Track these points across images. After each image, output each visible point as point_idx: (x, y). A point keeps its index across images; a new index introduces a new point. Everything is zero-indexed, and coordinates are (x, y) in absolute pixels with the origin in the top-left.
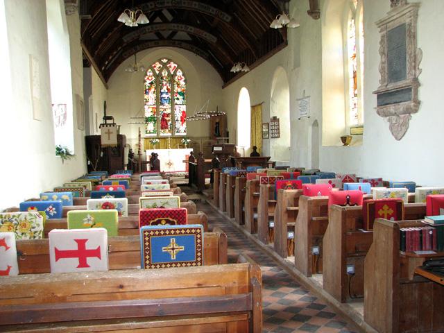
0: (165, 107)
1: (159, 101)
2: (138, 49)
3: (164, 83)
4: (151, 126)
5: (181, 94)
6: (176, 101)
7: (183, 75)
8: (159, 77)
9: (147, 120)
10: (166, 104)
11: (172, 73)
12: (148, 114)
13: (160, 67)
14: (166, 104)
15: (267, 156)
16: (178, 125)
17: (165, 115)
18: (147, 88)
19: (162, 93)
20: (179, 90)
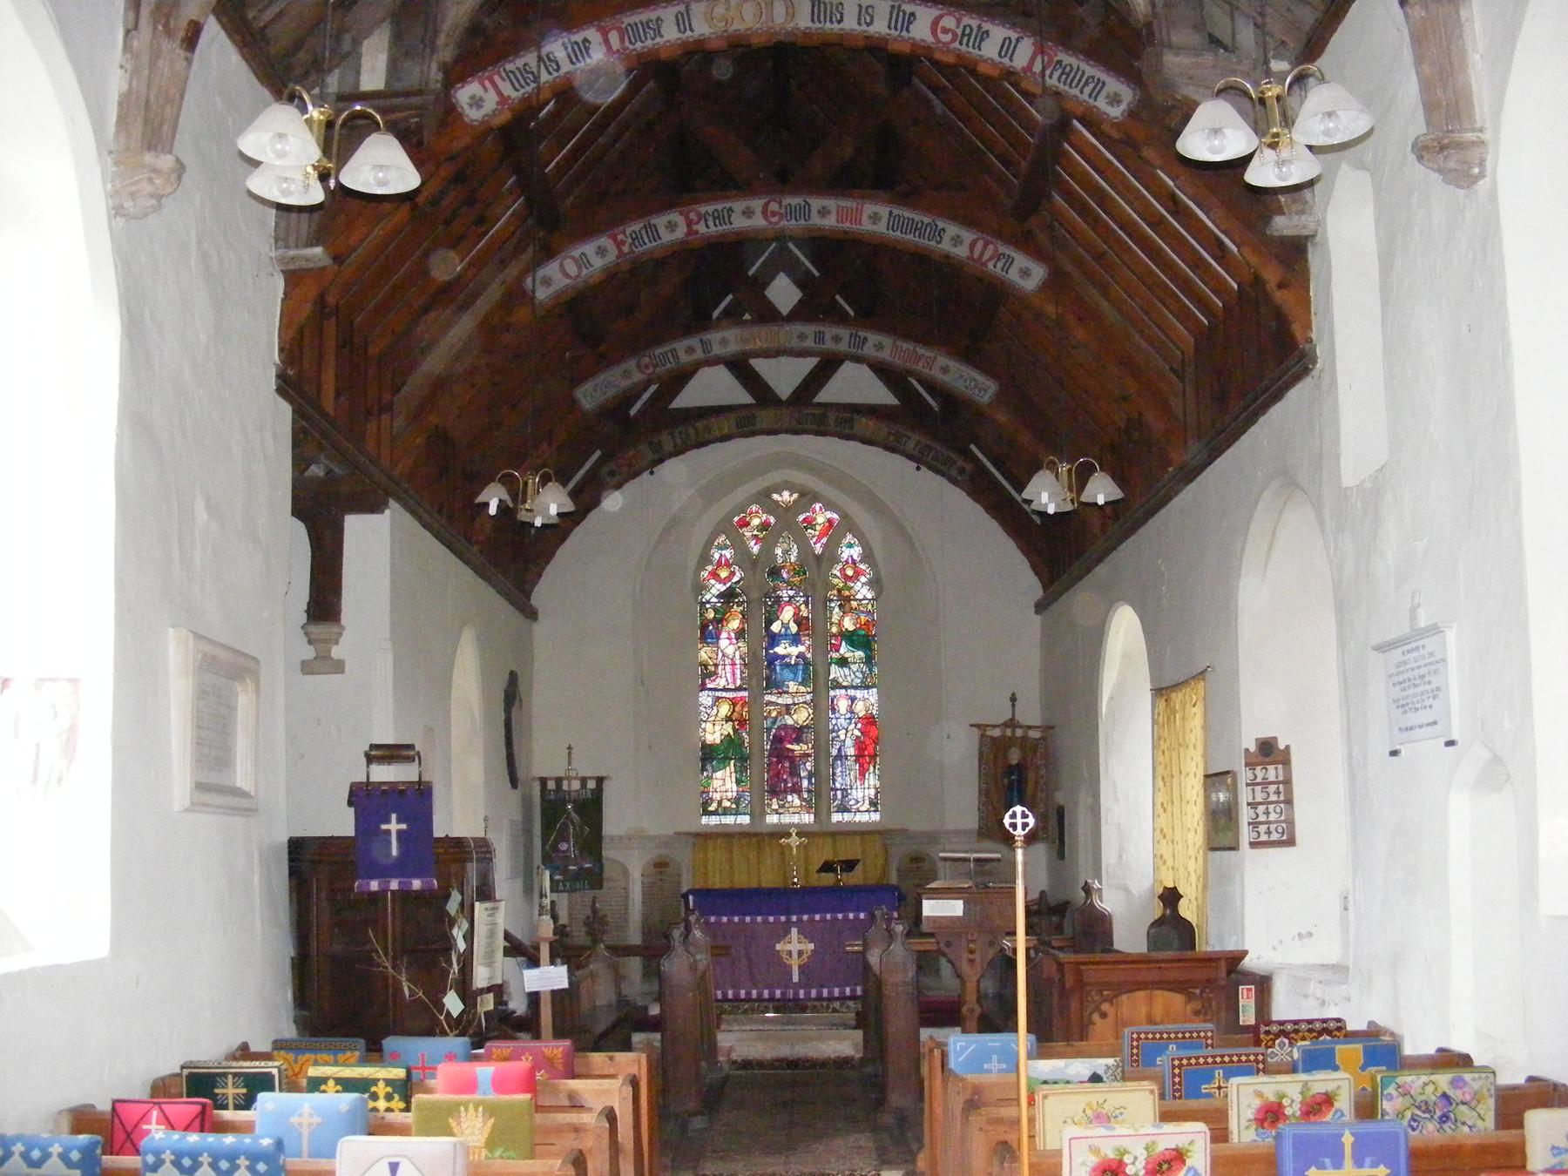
1: (764, 672)
2: (668, 446)
3: (785, 594)
4: (724, 783)
7: (868, 557)
9: (710, 756)
11: (818, 549)
12: (714, 733)
13: (764, 526)
15: (1230, 945)
16: (845, 776)
18: (711, 615)
19: (774, 639)
20: (849, 624)
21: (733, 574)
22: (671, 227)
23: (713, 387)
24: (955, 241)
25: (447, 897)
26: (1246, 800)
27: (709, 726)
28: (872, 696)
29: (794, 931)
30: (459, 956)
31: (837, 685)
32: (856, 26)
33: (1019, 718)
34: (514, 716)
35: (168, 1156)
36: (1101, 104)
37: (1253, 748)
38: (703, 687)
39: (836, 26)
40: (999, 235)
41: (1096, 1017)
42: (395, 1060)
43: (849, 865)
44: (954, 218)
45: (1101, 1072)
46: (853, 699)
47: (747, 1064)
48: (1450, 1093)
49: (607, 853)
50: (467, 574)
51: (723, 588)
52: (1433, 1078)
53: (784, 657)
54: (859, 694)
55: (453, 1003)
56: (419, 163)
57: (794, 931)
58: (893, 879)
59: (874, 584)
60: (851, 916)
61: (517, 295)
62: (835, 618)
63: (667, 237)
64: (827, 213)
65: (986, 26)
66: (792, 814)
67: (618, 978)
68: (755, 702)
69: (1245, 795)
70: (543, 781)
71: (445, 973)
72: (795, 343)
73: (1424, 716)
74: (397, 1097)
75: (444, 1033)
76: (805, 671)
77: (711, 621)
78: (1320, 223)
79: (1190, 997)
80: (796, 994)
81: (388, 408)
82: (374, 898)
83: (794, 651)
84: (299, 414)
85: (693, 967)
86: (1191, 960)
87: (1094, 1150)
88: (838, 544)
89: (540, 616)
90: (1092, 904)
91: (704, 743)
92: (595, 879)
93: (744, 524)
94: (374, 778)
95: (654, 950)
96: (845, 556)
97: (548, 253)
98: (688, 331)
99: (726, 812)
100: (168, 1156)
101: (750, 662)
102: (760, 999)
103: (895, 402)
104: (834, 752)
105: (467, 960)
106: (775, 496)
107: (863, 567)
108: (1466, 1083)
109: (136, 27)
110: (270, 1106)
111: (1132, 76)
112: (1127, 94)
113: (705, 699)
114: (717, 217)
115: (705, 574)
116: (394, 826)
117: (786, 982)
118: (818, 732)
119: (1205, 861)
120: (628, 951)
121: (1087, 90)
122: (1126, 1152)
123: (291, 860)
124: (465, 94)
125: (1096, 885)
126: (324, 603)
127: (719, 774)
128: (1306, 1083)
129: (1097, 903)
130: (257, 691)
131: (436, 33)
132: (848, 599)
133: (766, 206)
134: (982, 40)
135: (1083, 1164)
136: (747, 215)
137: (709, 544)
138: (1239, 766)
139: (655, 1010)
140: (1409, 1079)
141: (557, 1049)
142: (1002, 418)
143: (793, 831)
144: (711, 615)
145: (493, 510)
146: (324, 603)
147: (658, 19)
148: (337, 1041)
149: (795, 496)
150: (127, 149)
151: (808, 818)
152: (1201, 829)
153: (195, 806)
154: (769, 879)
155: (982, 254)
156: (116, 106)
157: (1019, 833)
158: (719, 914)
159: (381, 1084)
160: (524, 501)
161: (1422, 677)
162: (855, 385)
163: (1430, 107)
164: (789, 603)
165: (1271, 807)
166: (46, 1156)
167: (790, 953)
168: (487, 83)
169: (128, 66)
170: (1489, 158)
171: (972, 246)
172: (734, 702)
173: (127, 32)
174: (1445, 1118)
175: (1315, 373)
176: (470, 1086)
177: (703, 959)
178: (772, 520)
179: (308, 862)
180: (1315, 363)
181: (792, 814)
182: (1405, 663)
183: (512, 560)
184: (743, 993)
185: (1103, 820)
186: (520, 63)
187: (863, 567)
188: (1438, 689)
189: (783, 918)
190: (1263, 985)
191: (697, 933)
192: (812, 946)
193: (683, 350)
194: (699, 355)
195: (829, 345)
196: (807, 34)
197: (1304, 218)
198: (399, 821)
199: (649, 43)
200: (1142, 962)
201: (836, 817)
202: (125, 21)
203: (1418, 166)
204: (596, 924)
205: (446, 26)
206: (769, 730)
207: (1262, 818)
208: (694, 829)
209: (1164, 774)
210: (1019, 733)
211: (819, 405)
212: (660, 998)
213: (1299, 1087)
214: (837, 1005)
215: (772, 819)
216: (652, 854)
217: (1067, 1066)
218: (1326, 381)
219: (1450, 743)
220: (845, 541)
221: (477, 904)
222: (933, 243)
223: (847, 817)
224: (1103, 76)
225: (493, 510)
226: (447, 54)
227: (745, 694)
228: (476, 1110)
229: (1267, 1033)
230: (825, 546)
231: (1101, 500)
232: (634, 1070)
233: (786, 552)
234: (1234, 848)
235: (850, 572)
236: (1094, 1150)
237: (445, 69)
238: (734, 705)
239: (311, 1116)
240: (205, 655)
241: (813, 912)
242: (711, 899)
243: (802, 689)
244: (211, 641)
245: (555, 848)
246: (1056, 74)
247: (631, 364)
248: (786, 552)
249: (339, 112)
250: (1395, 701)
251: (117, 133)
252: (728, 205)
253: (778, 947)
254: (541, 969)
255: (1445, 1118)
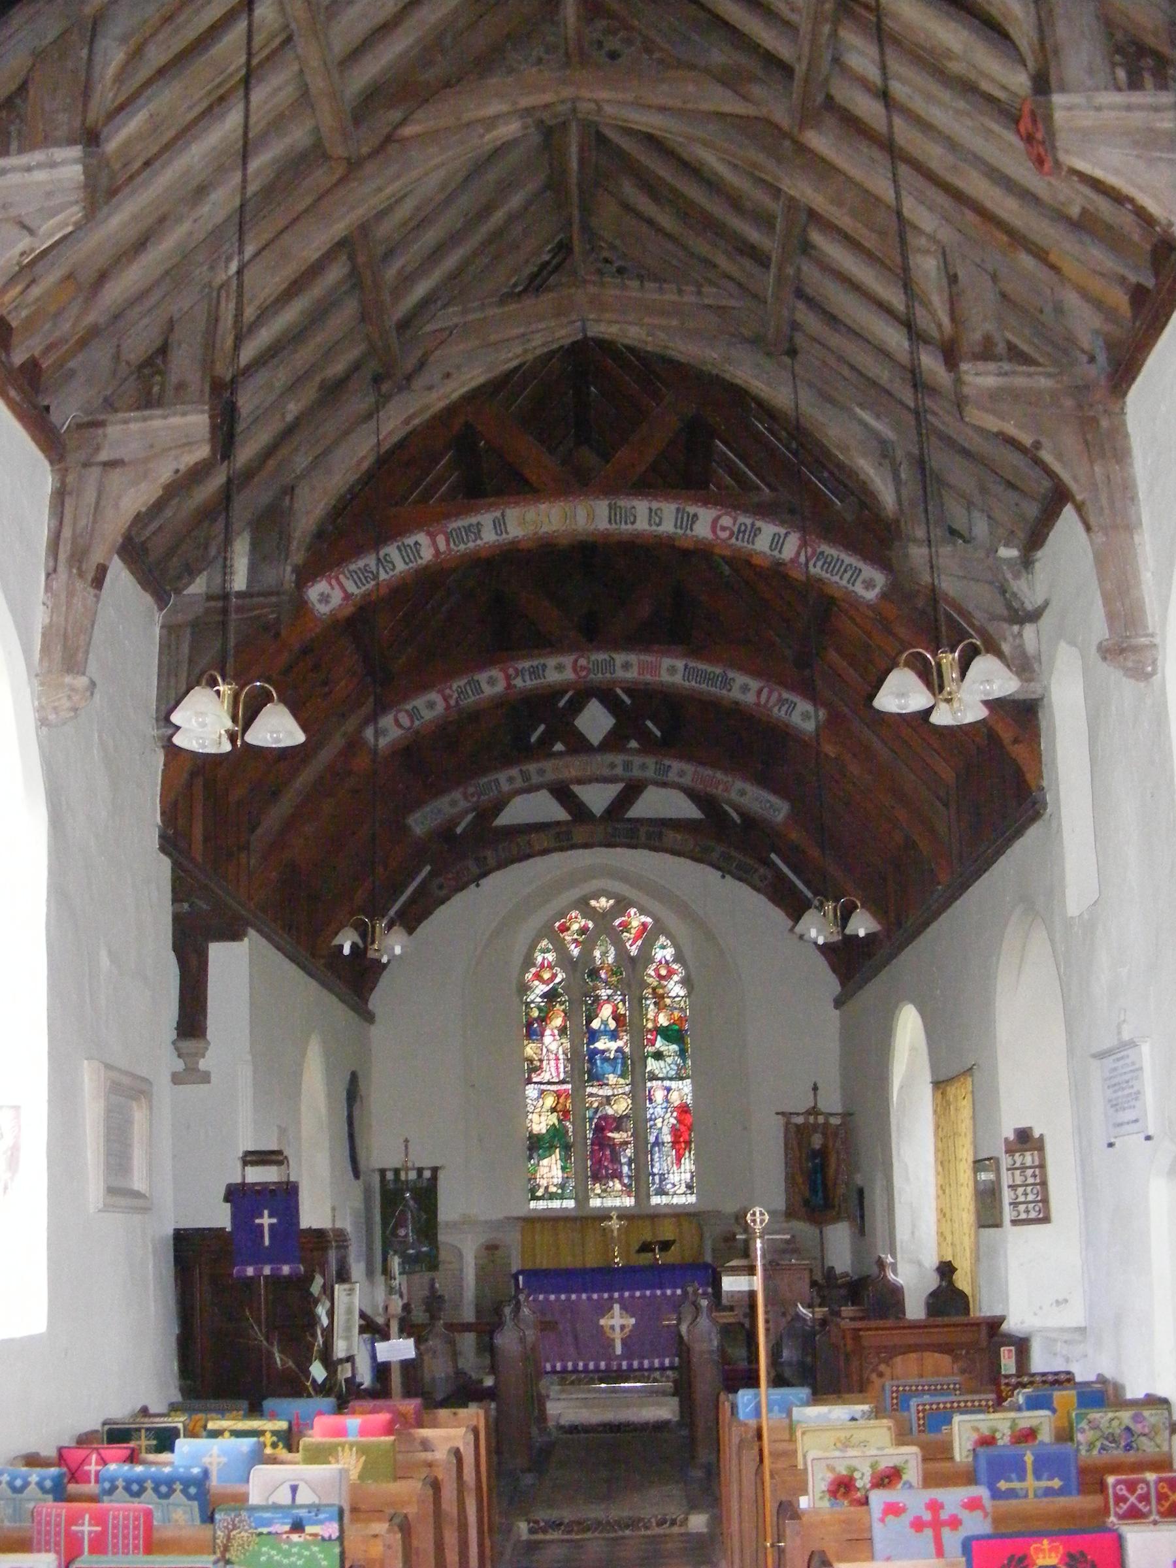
0: (607, 1091)
1: (585, 1066)
2: (492, 862)
3: (604, 993)
4: (550, 1170)
5: (672, 1034)
6: (652, 1065)
7: (678, 958)
8: (584, 973)
9: (537, 1145)
10: (612, 1079)
11: (634, 951)
12: (541, 1123)
13: (583, 931)
14: (612, 1079)
15: (997, 1312)
16: (662, 1162)
17: (605, 1125)
18: (535, 1013)
19: (593, 1036)
20: (663, 1020)
21: (555, 976)
22: (492, 682)
23: (535, 808)
24: (744, 689)
25: (311, 1279)
26: (1008, 1183)
27: (535, 1117)
28: (686, 1087)
29: (617, 1307)
30: (323, 1330)
31: (654, 1077)
32: (647, 527)
33: (823, 1106)
34: (356, 1113)
35: (120, 1483)
36: (859, 589)
37: (1012, 1137)
38: (529, 1081)
39: (629, 526)
40: (783, 684)
41: (874, 1376)
42: (273, 1416)
43: (665, 1246)
44: (742, 669)
45: (857, 1416)
46: (669, 1090)
47: (573, 1429)
48: (1132, 1426)
49: (442, 1237)
50: (313, 984)
51: (547, 988)
52: (1117, 1414)
53: (603, 1052)
54: (673, 1084)
55: (318, 1371)
56: (305, 728)
57: (617, 1307)
58: (708, 1258)
59: (686, 982)
60: (669, 1292)
61: (354, 744)
62: (651, 1015)
63: (488, 691)
64: (628, 667)
65: (759, 524)
66: (613, 1198)
67: (455, 1355)
68: (578, 1094)
69: (1006, 1179)
70: (382, 1172)
71: (310, 1346)
72: (606, 772)
73: (1128, 1115)
74: (281, 1445)
75: (309, 1396)
76: (624, 1064)
77: (536, 1020)
78: (1046, 688)
79: (956, 1358)
80: (620, 1365)
81: (246, 847)
82: (250, 1283)
83: (613, 1045)
84: (177, 866)
85: (522, 1340)
86: (966, 1325)
87: (831, 1469)
88: (652, 946)
89: (377, 1018)
90: (885, 1276)
91: (531, 1132)
92: (431, 1262)
93: (565, 929)
94: (249, 1180)
95: (487, 1326)
96: (658, 957)
97: (381, 708)
98: (507, 761)
99: (552, 1197)
100: (120, 1483)
101: (573, 1058)
102: (586, 1370)
103: (703, 816)
104: (652, 1139)
105: (329, 1333)
106: (593, 903)
107: (675, 966)
108: (1144, 1418)
109: (55, 570)
110: (186, 1449)
111: (884, 564)
112: (881, 579)
113: (531, 1091)
114: (534, 672)
115: (529, 976)
116: (266, 1221)
117: (610, 1357)
118: (638, 1120)
119: (977, 1235)
120: (466, 1327)
121: (847, 576)
122: (855, 1470)
123: (176, 1250)
124: (314, 592)
125: (890, 1259)
126: (192, 1021)
127: (545, 1162)
128: (1014, 1420)
129: (891, 1276)
130: (151, 1108)
131: (289, 538)
132: (662, 997)
133: (576, 661)
134: (755, 535)
135: (823, 1479)
136: (557, 670)
137: (532, 948)
138: (1000, 1152)
139: (489, 1382)
140: (1098, 1415)
141: (410, 1406)
142: (794, 836)
143: (614, 1214)
144: (535, 1013)
145: (347, 951)
146: (192, 1021)
147: (478, 523)
148: (222, 1403)
149: (612, 902)
150: (50, 671)
151: (629, 1202)
152: (972, 1208)
153: (106, 1208)
154: (592, 1260)
155: (767, 701)
156: (40, 636)
157: (758, 1228)
158: (547, 1292)
159: (268, 1435)
160: (373, 942)
161: (1127, 1082)
162: (661, 803)
163: (1111, 617)
164: (608, 1001)
165: (1029, 1188)
166: (26, 1484)
167: (612, 1327)
168: (334, 582)
169: (49, 603)
170: (1160, 658)
171: (759, 692)
172: (558, 1095)
173: (48, 575)
174: (1128, 1447)
175: (1046, 816)
176: (342, 1432)
177: (531, 1334)
178: (591, 925)
179: (191, 1251)
180: (1045, 809)
181: (613, 1198)
182: (1115, 1069)
183: (356, 979)
184: (570, 1365)
185: (896, 1201)
186: (361, 563)
187: (675, 966)
188: (1139, 1092)
189: (606, 1296)
190: (1022, 1346)
191: (526, 1311)
192: (633, 1321)
193: (505, 778)
194: (519, 783)
195: (636, 773)
196: (606, 535)
197: (1032, 684)
198: (270, 1216)
199: (471, 545)
200: (920, 1327)
201: (655, 1200)
202: (46, 569)
203: (1105, 665)
204: (434, 1302)
205: (297, 534)
206: (591, 1119)
207: (1022, 1199)
208: (521, 1213)
209: (944, 1161)
210: (821, 1120)
211: (630, 820)
212: (493, 1370)
213: (1008, 1424)
214: (657, 1374)
215: (595, 1203)
216: (482, 1239)
217: (830, 1412)
218: (1054, 825)
219: (1148, 1138)
220: (658, 944)
221: (337, 1286)
222: (724, 692)
223: (664, 1200)
224: (860, 564)
225: (347, 951)
226: (298, 557)
227: (569, 1086)
228: (351, 1450)
229: (1007, 1384)
230: (640, 949)
231: (862, 933)
232: (474, 1423)
233: (604, 954)
234: (998, 1225)
235: (663, 972)
236: (831, 1469)
237: (297, 570)
238: (559, 1096)
239: (219, 1456)
240: (113, 1082)
241: (632, 1289)
242: (539, 1278)
243: (622, 1081)
244: (119, 1070)
245: (394, 1233)
246: (820, 564)
247: (457, 795)
248: (604, 955)
249: (242, 688)
250: (1110, 1101)
251: (41, 660)
252: (542, 661)
253: (602, 1322)
254: (393, 1341)
255: (1128, 1447)
